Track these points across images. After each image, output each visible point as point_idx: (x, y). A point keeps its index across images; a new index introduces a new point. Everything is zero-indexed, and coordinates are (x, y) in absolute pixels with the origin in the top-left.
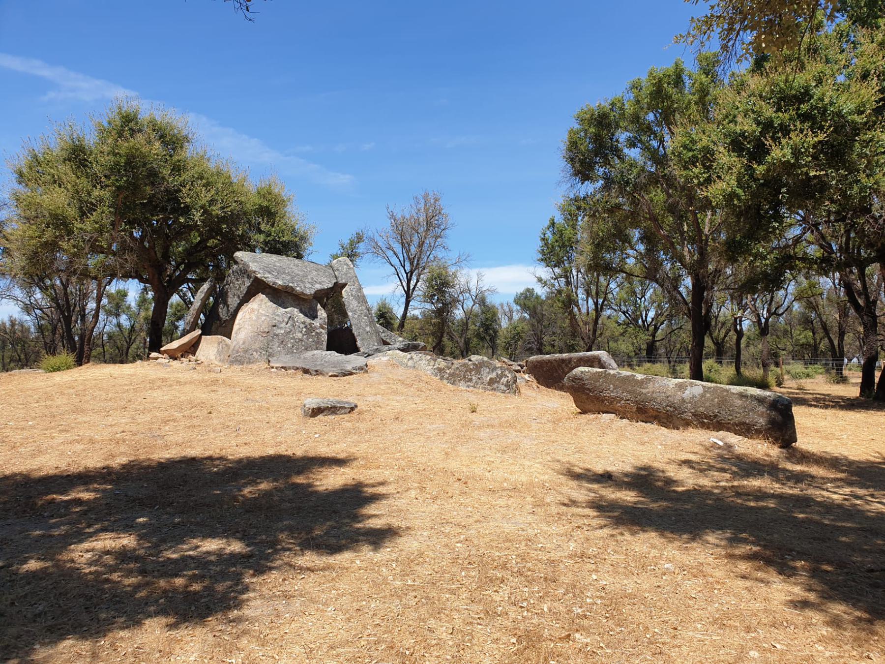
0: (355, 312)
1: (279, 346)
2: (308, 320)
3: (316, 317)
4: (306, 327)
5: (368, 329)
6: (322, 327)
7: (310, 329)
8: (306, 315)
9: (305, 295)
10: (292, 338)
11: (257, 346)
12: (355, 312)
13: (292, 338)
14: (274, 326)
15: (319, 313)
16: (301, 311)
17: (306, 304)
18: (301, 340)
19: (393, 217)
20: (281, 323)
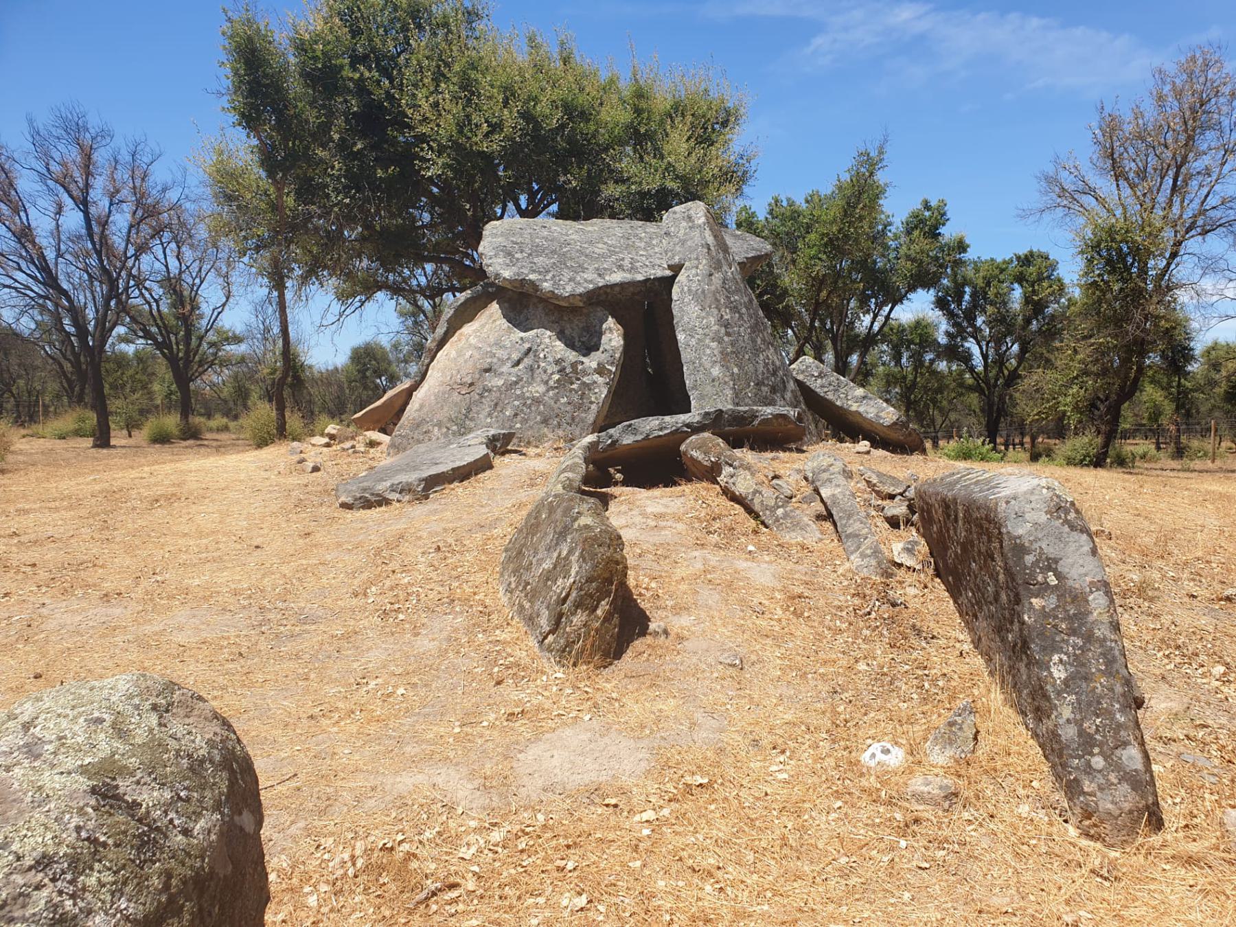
0: (691, 332)
1: (490, 415)
2: (572, 356)
3: (596, 348)
4: (562, 370)
5: (716, 371)
6: (600, 370)
7: (568, 375)
8: (570, 345)
9: (557, 297)
10: (518, 397)
11: (442, 415)
12: (691, 332)
13: (518, 397)
14: (487, 370)
15: (604, 339)
16: (561, 336)
17: (575, 319)
18: (537, 401)
19: (30, 122)
20: (503, 362)
